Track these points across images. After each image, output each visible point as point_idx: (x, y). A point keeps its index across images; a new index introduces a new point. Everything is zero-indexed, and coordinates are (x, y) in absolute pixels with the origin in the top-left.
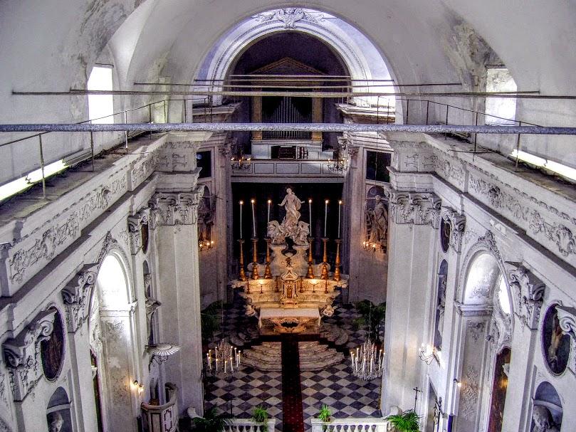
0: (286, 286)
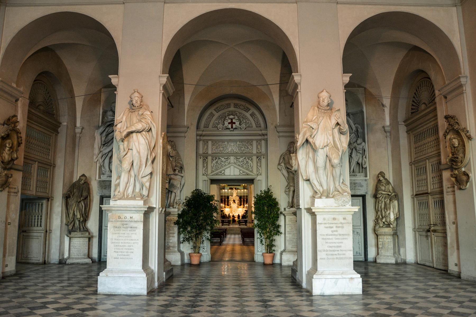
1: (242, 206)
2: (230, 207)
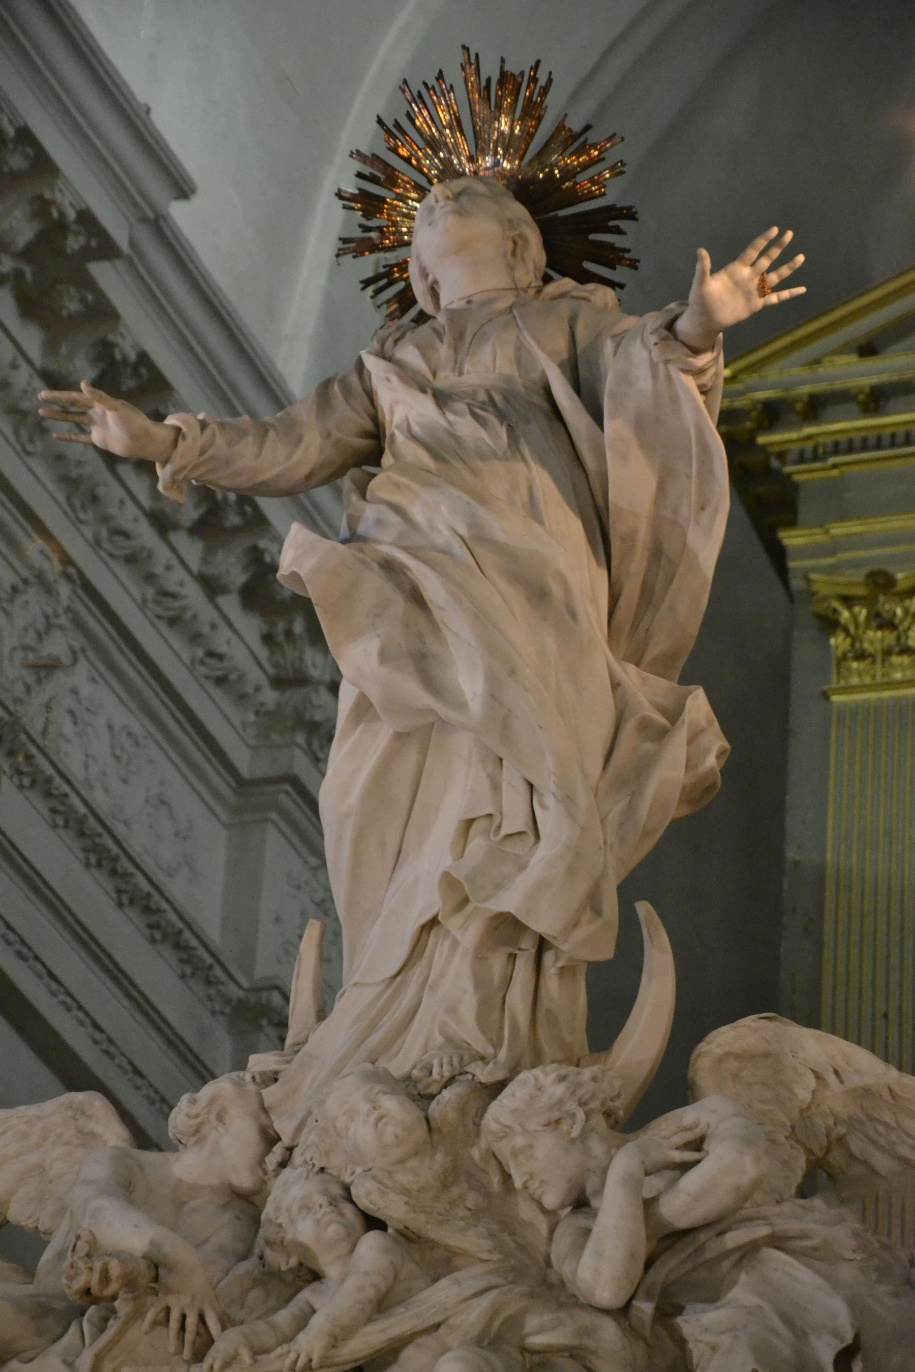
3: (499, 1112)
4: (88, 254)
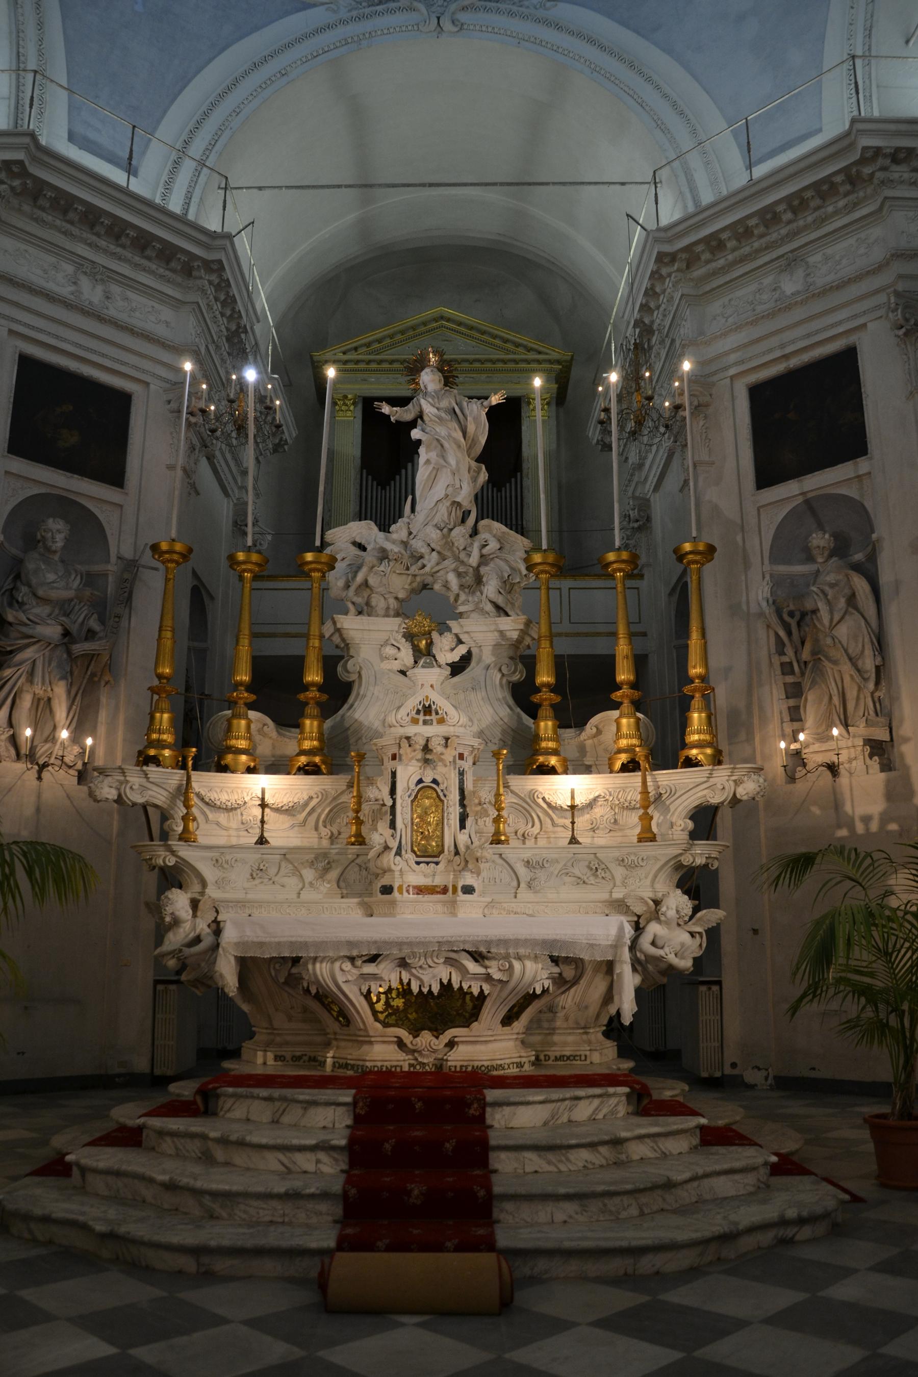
0: (409, 773)
1: (618, 728)
2: (337, 756)
3: (454, 533)
4: (243, 332)
